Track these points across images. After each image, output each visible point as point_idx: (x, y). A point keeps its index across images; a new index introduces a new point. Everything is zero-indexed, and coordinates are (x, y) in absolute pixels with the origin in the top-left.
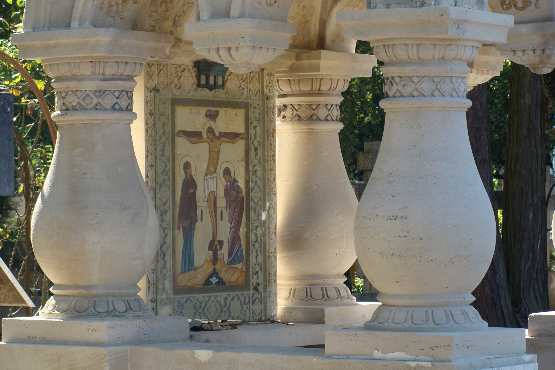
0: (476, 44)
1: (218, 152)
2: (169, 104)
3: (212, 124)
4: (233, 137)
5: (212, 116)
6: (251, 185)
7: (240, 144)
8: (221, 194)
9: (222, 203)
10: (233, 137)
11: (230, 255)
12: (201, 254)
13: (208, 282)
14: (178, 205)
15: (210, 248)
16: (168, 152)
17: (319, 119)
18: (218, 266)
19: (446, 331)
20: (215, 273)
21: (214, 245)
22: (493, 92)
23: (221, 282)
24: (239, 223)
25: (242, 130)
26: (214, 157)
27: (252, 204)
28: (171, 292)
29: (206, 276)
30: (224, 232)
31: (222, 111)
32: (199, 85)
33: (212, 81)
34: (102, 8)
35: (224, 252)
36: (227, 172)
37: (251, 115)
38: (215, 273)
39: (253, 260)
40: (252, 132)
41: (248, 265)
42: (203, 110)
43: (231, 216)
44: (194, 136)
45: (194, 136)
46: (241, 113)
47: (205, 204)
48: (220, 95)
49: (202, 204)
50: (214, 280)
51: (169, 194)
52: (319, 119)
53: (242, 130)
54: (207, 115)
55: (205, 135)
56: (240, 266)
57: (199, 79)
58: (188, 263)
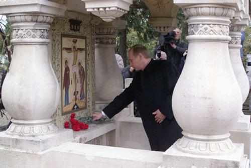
0: (52, 16)
1: (77, 56)
2: (60, 36)
3: (75, 45)
4: (81, 50)
5: (75, 42)
6: (87, 68)
7: (84, 52)
8: (78, 73)
9: (78, 76)
10: (81, 50)
11: (80, 96)
12: (71, 97)
13: (74, 108)
14: (63, 78)
15: (74, 95)
16: (60, 57)
17: (109, 44)
18: (77, 102)
19: (181, 157)
20: (76, 104)
21: (75, 94)
22: (172, 37)
23: (78, 107)
24: (83, 84)
25: (84, 48)
26: (76, 58)
27: (87, 76)
28: (60, 114)
29: (73, 106)
30: (79, 89)
31: (78, 40)
32: (71, 29)
33: (75, 28)
34: (111, 134)
35: (78, 96)
36: (80, 64)
37: (87, 42)
38: (76, 104)
39: (88, 97)
40: (87, 48)
41: (86, 99)
42: (72, 39)
43: (81, 80)
44: (68, 49)
45: (68, 49)
46: (84, 40)
47: (72, 77)
48: (78, 33)
49: (71, 77)
50: (76, 107)
51: (60, 74)
52: (109, 44)
53: (84, 48)
54: (73, 41)
55: (72, 49)
56: (83, 100)
57: (71, 26)
58: (67, 103)
